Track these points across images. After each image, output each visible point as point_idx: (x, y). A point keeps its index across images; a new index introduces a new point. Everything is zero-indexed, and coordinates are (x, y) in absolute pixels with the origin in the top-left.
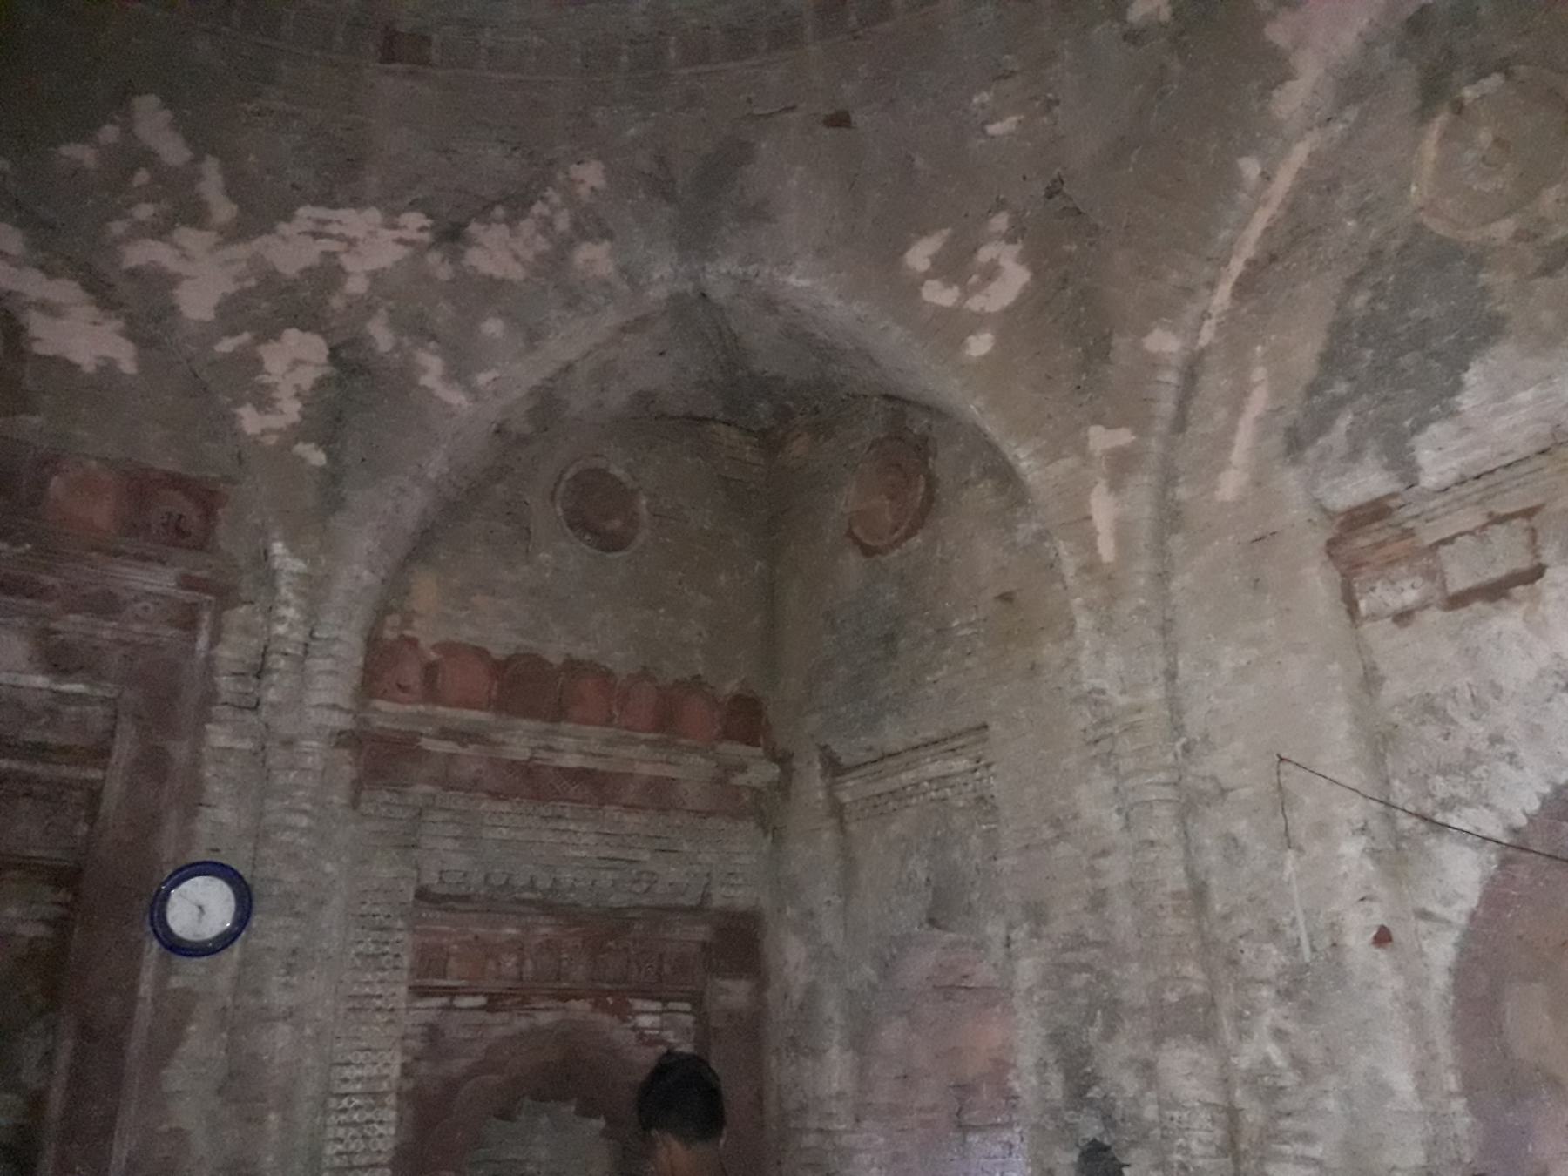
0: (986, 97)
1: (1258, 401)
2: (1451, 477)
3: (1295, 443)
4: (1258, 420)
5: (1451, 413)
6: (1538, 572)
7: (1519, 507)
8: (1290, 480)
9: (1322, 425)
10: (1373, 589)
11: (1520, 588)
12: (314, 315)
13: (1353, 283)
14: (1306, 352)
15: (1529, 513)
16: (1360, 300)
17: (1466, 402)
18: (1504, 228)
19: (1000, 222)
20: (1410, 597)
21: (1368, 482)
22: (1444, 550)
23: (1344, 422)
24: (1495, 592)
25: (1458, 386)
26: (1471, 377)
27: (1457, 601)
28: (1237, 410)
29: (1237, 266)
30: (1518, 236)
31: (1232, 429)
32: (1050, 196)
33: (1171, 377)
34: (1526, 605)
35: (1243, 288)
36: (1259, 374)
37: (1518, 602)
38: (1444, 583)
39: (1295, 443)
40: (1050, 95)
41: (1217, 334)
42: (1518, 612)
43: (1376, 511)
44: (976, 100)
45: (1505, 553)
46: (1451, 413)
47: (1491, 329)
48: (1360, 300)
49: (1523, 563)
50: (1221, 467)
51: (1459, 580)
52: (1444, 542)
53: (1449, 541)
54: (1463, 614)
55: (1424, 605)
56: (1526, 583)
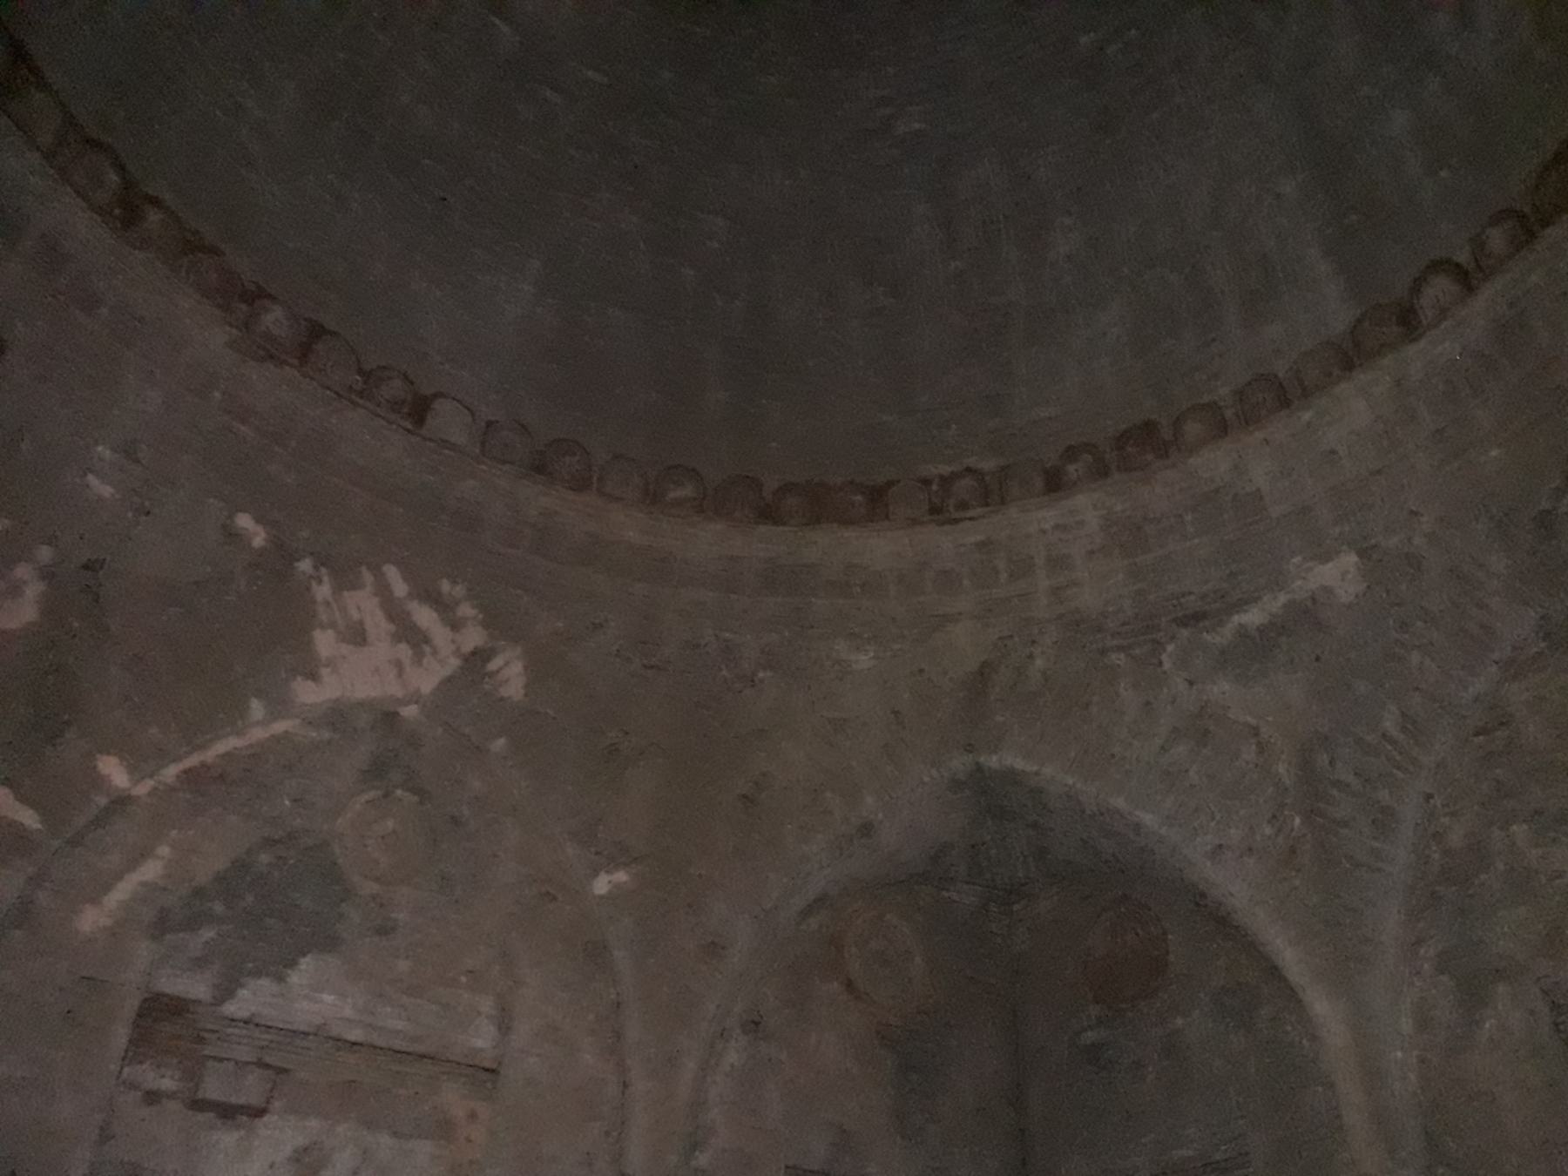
0: (108, 454)
1: (150, 871)
2: (245, 1014)
3: (162, 926)
4: (144, 884)
5: (280, 979)
6: (260, 1112)
7: (279, 1064)
8: (144, 951)
9: (192, 924)
10: (141, 1063)
11: (245, 1118)
12: (1035, 825)
13: (269, 843)
14: (210, 864)
15: (282, 1071)
16: (265, 858)
17: (295, 978)
18: (371, 888)
19: (45, 553)
20: (167, 1084)
21: (196, 987)
22: (210, 1063)
23: (208, 934)
24: (228, 1113)
25: (292, 964)
26: (306, 963)
27: (198, 1105)
28: (133, 863)
29: (193, 761)
30: (374, 897)
31: (119, 876)
32: (86, 567)
33: (103, 801)
34: (242, 1132)
35: (191, 778)
36: (164, 850)
37: (238, 1127)
38: (197, 1085)
39: (162, 926)
40: (147, 504)
41: (149, 794)
42: (236, 1135)
43: (177, 1008)
44: (100, 448)
45: (251, 1089)
46: (280, 979)
47: (327, 942)
48: (265, 858)
49: (255, 1100)
50: (95, 901)
51: (212, 1089)
52: (215, 1058)
53: (221, 1060)
54: (201, 1117)
55: (171, 1096)
56: (249, 1115)
